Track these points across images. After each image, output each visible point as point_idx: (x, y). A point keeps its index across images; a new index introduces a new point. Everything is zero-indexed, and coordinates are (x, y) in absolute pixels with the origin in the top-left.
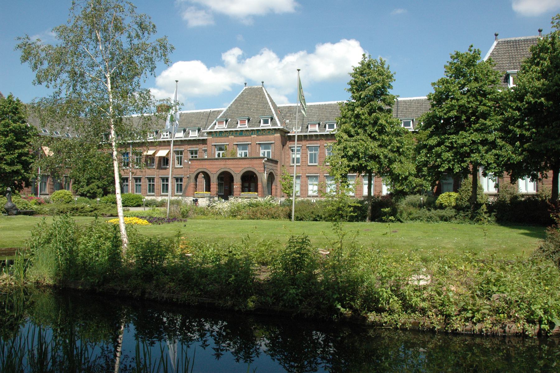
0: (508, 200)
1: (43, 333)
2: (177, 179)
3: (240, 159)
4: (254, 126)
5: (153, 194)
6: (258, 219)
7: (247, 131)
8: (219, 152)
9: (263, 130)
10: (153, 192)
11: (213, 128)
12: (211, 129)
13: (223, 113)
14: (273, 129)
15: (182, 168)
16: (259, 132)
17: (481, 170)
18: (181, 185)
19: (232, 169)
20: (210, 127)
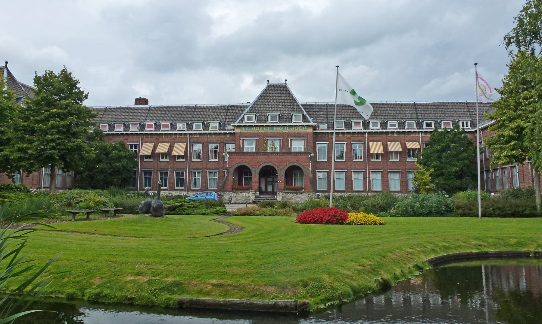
0: (57, 73)
1: (254, 249)
2: (146, 173)
3: (271, 153)
4: (286, 122)
5: (134, 188)
6: (282, 216)
7: (278, 126)
8: (248, 146)
9: (295, 126)
10: (182, 186)
11: (242, 121)
12: (239, 123)
13: (250, 107)
14: (306, 125)
15: (201, 161)
16: (291, 128)
17: (116, 193)
18: (182, 179)
19: (276, 163)
20: (238, 121)
